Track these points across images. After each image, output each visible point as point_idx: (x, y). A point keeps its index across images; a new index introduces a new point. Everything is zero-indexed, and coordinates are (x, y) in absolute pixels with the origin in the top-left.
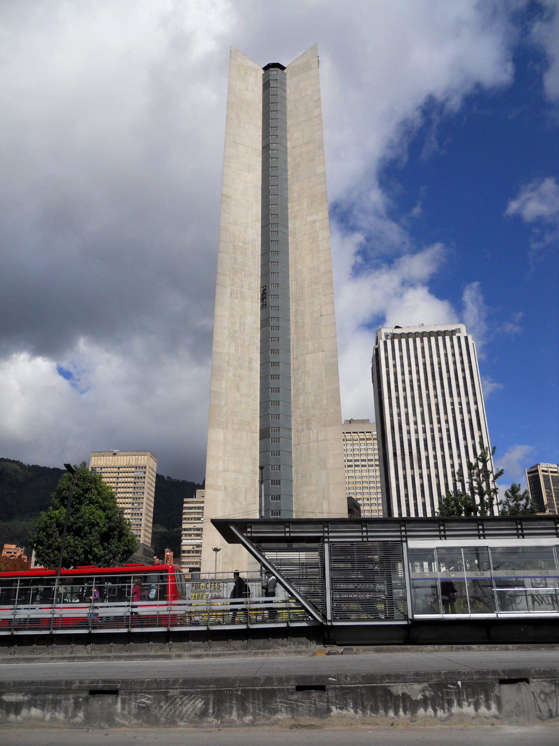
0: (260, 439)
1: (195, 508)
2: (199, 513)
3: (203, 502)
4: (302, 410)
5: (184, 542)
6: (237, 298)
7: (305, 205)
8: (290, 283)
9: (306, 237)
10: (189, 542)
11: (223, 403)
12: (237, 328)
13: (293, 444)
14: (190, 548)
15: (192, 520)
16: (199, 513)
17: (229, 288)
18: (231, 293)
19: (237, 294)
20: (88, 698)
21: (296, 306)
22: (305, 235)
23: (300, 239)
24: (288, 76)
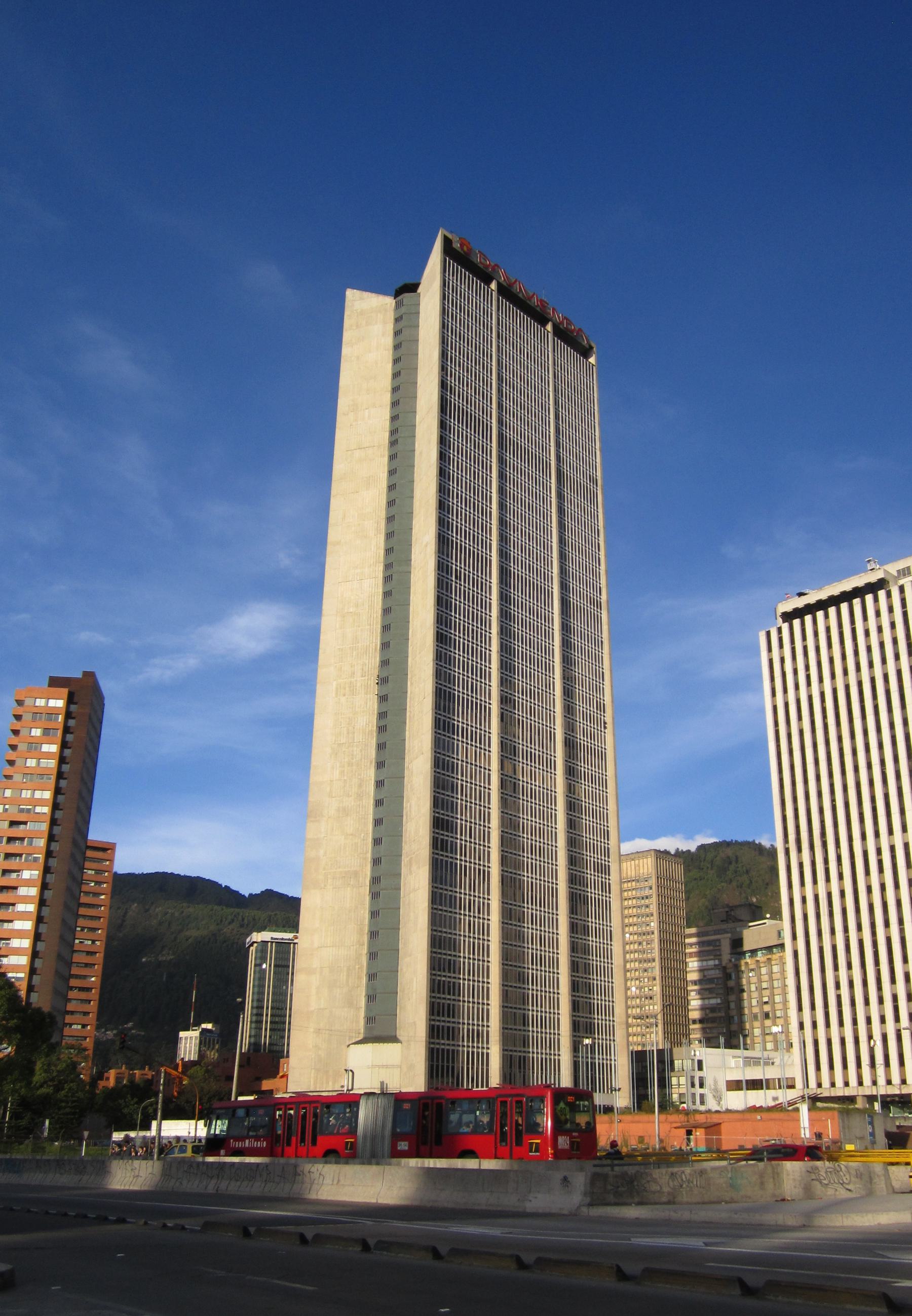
11: (322, 852)
12: (343, 741)
18: (337, 689)
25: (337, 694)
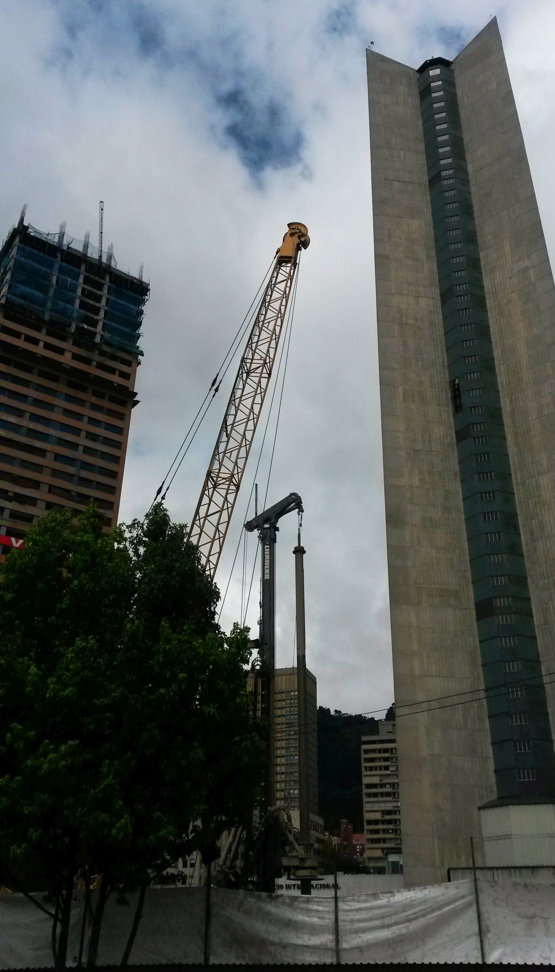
0: (478, 619)
1: (380, 751)
2: (386, 759)
3: (393, 741)
4: (544, 566)
5: (367, 807)
6: (414, 402)
7: (507, 249)
8: (497, 369)
9: (513, 295)
10: (376, 807)
12: (419, 447)
13: (536, 623)
14: (378, 816)
15: (376, 770)
16: (386, 759)
17: (401, 389)
18: (404, 395)
19: (414, 396)
20: (190, 877)
21: (511, 401)
22: (513, 292)
23: (505, 301)
24: (456, 74)
25: (404, 398)
